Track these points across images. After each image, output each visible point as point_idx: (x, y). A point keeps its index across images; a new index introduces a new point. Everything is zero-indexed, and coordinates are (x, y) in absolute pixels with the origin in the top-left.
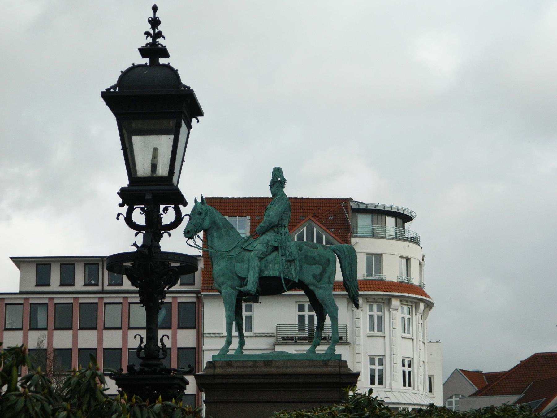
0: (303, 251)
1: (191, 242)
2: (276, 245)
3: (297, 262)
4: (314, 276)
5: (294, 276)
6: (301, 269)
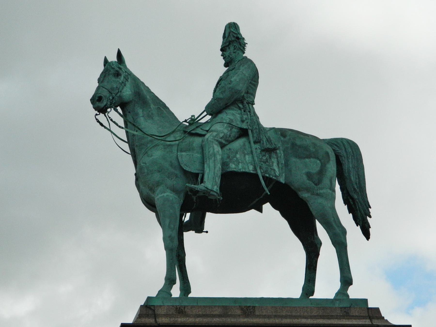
0: (288, 137)
1: (102, 117)
2: (244, 126)
3: (280, 152)
4: (309, 175)
5: (277, 174)
6: (287, 164)
